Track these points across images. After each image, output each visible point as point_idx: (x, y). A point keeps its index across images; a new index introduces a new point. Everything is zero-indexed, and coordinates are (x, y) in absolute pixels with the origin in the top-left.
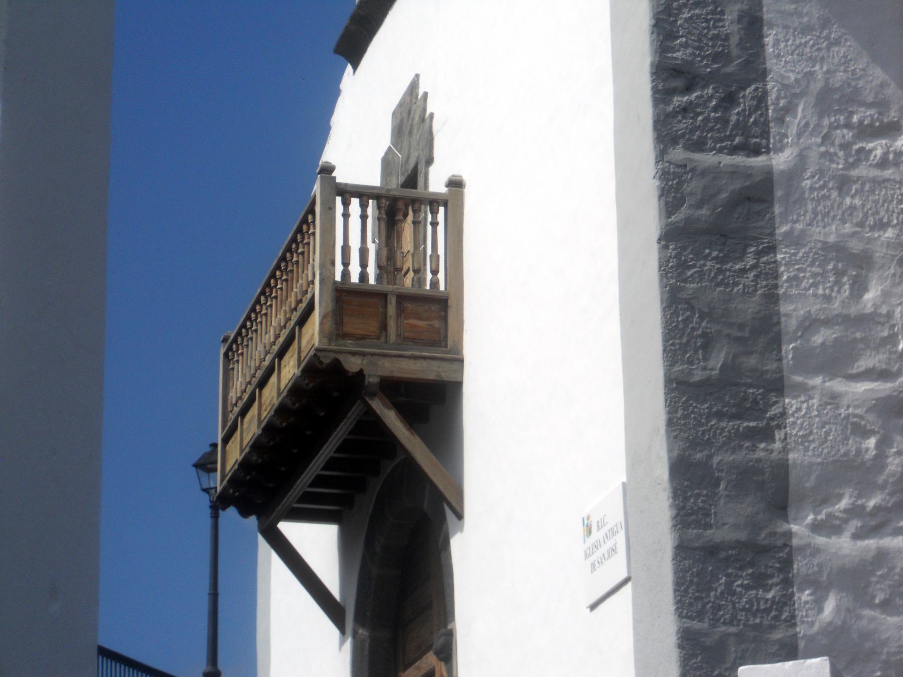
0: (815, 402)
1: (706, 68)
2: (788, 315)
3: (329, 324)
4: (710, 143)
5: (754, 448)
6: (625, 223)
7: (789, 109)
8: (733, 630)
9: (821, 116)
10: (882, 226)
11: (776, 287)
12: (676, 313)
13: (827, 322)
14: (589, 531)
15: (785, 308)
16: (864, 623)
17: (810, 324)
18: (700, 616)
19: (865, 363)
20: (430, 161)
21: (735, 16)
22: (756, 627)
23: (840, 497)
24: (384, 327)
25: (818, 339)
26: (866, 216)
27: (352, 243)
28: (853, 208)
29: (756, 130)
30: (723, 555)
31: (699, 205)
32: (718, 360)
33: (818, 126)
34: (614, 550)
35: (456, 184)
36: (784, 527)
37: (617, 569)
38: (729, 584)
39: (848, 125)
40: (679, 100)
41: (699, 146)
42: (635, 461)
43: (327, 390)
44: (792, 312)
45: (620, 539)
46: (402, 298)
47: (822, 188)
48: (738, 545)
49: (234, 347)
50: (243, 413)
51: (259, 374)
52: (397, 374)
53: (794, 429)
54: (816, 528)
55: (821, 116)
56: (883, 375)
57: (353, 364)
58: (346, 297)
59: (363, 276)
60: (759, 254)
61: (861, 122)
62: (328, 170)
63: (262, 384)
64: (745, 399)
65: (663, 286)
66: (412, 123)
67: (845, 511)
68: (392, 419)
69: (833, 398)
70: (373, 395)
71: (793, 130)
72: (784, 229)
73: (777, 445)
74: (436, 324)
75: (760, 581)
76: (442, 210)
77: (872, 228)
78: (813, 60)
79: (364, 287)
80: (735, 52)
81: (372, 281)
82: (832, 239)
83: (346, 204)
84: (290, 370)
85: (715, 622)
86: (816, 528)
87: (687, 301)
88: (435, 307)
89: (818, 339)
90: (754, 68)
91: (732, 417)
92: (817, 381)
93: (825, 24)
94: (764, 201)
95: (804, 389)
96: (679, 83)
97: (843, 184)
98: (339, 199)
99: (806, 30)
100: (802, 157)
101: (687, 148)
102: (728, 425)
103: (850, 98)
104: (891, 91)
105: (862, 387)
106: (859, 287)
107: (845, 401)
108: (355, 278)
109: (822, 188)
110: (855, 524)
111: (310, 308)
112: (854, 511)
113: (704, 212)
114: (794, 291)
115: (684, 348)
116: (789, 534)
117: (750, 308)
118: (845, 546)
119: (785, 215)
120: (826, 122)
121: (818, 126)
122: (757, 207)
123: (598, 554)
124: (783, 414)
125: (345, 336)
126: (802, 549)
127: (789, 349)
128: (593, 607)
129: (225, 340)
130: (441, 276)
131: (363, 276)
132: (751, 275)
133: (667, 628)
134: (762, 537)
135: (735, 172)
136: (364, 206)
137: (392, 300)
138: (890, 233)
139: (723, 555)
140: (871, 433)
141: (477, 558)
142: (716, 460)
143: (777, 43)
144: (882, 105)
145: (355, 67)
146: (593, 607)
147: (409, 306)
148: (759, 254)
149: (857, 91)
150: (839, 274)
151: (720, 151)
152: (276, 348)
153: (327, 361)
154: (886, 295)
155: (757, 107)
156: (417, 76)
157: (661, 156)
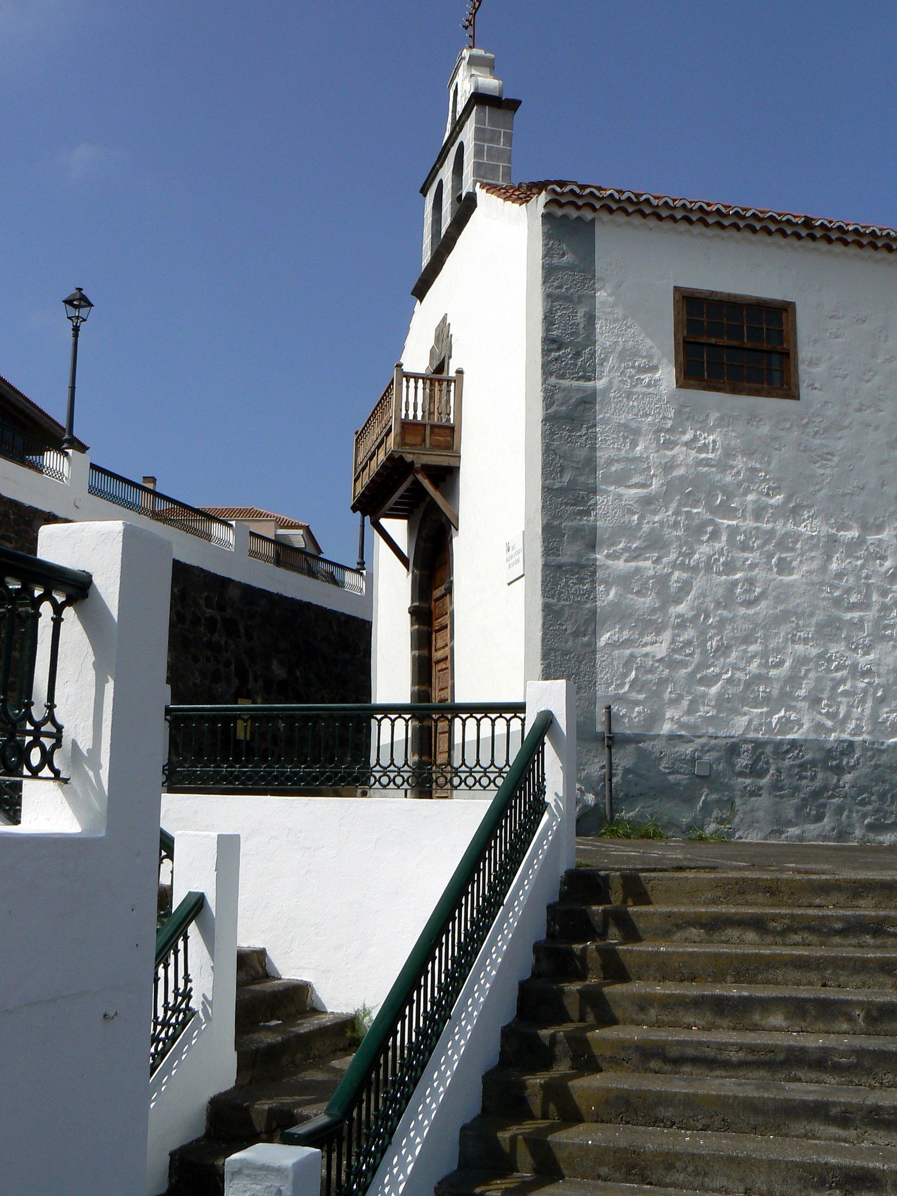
0: (611, 498)
1: (567, 339)
2: (600, 457)
3: (398, 438)
4: (568, 375)
5: (581, 520)
6: (528, 410)
7: (605, 359)
8: (567, 603)
9: (620, 362)
10: (646, 415)
11: (595, 444)
12: (548, 456)
13: (618, 461)
15: (599, 454)
16: (628, 601)
17: (610, 462)
18: (553, 597)
19: (634, 480)
20: (450, 357)
21: (582, 314)
22: (578, 602)
23: (620, 542)
24: (424, 440)
25: (613, 469)
26: (639, 411)
27: (413, 401)
28: (633, 406)
29: (590, 369)
30: (564, 569)
31: (562, 405)
32: (566, 478)
33: (619, 367)
34: (518, 561)
35: (460, 372)
36: (594, 556)
38: (567, 582)
39: (633, 367)
40: (554, 355)
41: (562, 377)
43: (395, 470)
44: (602, 455)
46: (433, 427)
47: (619, 397)
48: (572, 564)
49: (360, 436)
50: (363, 469)
51: (370, 454)
52: (429, 463)
53: (600, 510)
54: (608, 556)
55: (620, 362)
56: (643, 486)
57: (409, 458)
58: (407, 426)
59: (415, 416)
60: (588, 428)
61: (639, 366)
62: (400, 366)
63: (371, 459)
64: (578, 496)
65: (543, 443)
66: (443, 335)
67: (622, 549)
68: (426, 484)
69: (619, 497)
70: (418, 472)
71: (607, 370)
72: (601, 416)
73: (592, 518)
74: (449, 439)
75: (581, 581)
76: (453, 384)
77: (642, 417)
78: (618, 335)
79: (415, 421)
80: (581, 331)
81: (419, 418)
82: (622, 422)
83: (408, 382)
84: (381, 457)
85: (559, 600)
86: (608, 556)
87: (554, 450)
88: (448, 431)
89: (613, 469)
90: (590, 340)
91: (572, 505)
92: (613, 488)
93: (625, 318)
94: (590, 403)
95: (606, 492)
96: (555, 346)
97: (629, 395)
98: (404, 379)
99: (616, 320)
100: (610, 382)
101: (557, 377)
102: (570, 509)
103: (634, 354)
104: (654, 350)
105: (633, 491)
106: (634, 444)
107: (624, 498)
108: (411, 417)
109: (619, 397)
110: (626, 555)
111: (390, 430)
112: (626, 549)
114: (603, 446)
115: (551, 472)
116: (596, 559)
117: (582, 454)
118: (620, 565)
119: (601, 410)
120: (623, 365)
121: (619, 367)
122: (588, 406)
123: (512, 561)
124: (596, 504)
125: (406, 444)
126: (600, 566)
127: (600, 473)
128: (509, 584)
129: (356, 433)
130: (452, 416)
131: (415, 416)
132: (584, 438)
134: (583, 561)
135: (579, 389)
136: (416, 383)
137: (428, 428)
138: (650, 419)
139: (564, 569)
140: (637, 513)
141: (463, 547)
142: (563, 525)
143: (601, 327)
144: (650, 357)
145: (421, 302)
146: (509, 584)
147: (436, 430)
148: (588, 428)
149: (638, 351)
150: (625, 438)
151: (572, 379)
152: (377, 444)
153: (396, 457)
154: (646, 448)
155: (591, 358)
156: (445, 318)
157: (544, 381)
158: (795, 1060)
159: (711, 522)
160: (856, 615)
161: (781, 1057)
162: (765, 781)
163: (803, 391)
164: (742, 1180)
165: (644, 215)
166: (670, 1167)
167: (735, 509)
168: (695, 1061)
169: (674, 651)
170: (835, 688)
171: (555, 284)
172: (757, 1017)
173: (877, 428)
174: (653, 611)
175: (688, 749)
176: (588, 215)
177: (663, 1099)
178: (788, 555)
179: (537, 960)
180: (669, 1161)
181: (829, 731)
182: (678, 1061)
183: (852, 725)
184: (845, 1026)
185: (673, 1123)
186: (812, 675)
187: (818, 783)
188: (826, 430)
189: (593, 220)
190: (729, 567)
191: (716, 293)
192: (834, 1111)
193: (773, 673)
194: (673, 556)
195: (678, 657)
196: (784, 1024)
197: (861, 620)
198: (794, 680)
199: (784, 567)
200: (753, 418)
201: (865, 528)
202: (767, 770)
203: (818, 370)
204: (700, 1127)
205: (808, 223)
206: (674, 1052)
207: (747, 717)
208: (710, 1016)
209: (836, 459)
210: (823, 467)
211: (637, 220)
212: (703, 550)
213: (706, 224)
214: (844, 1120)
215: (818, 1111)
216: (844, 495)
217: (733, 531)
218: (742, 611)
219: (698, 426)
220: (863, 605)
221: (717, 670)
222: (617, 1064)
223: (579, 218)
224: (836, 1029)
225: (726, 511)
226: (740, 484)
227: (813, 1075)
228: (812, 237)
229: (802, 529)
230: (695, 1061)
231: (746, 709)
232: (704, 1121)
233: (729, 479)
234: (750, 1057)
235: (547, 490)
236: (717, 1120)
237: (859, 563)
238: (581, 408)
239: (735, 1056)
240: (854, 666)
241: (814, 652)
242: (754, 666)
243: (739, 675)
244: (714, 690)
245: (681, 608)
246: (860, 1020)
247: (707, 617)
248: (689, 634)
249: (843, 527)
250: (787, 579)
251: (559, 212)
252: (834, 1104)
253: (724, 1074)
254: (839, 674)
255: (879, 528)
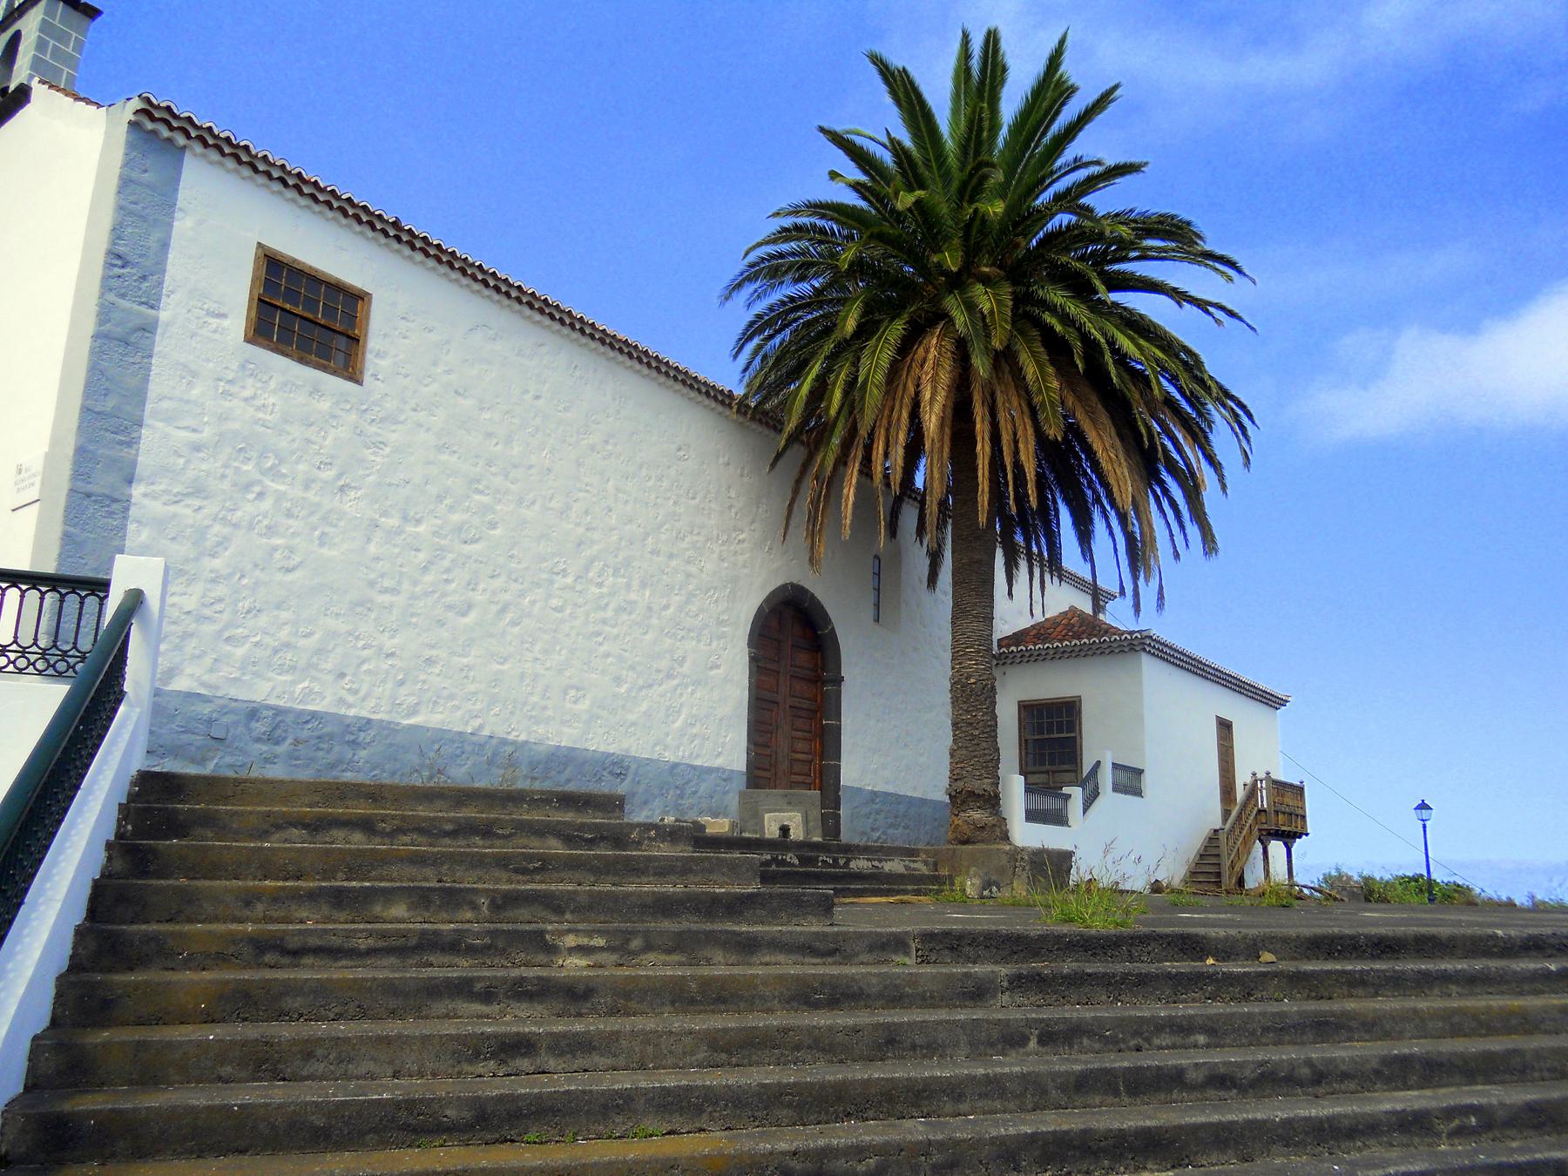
1: (134, 259)
6: (74, 324)
14: (20, 472)
15: (151, 386)
18: (75, 525)
19: (185, 424)
31: (117, 325)
37: (34, 494)
40: (117, 271)
41: (123, 296)
42: (55, 442)
44: (154, 389)
45: (38, 480)
69: (166, 436)
86: (145, 495)
92: (160, 425)
96: (119, 262)
105: (183, 434)
110: (165, 498)
113: (119, 329)
118: (157, 508)
133: (56, 529)
134: (116, 495)
135: (140, 314)
138: (211, 365)
157: (102, 295)
158: (430, 943)
159: (260, 482)
160: (387, 598)
161: (413, 941)
162: (281, 749)
163: (367, 378)
164: (391, 1062)
165: (240, 162)
166: (309, 1056)
167: (285, 476)
168: (317, 951)
169: (204, 605)
170: (359, 666)
171: (132, 198)
172: (377, 909)
173: (428, 430)
174: (187, 560)
175: (206, 710)
176: (181, 140)
177: (289, 988)
178: (328, 529)
179: (109, 859)
180: (308, 1050)
181: (350, 706)
182: (297, 953)
183: (372, 703)
184: (469, 915)
185: (301, 1015)
186: (338, 650)
187: (331, 758)
188: (382, 420)
189: (184, 148)
190: (271, 530)
191: (299, 262)
192: (478, 987)
193: (302, 642)
194: (215, 509)
195: (207, 612)
196: (406, 915)
197: (391, 606)
198: (320, 651)
199: (323, 540)
200: (316, 391)
201: (405, 518)
202: (285, 739)
203: (384, 363)
204: (332, 1016)
205: (396, 224)
206: (294, 943)
207: (271, 684)
208: (326, 910)
209: (388, 450)
210: (374, 453)
211: (231, 164)
212: (247, 509)
213: (301, 193)
214: (487, 996)
215: (462, 989)
216: (390, 485)
217: (280, 496)
218: (279, 576)
219: (259, 385)
220: (394, 591)
221: (246, 632)
222: (224, 960)
223: (169, 140)
224: (460, 918)
225: (274, 473)
226: (293, 453)
227: (446, 959)
228: (398, 239)
229: (346, 507)
230: (317, 951)
231: (271, 675)
232: (336, 1010)
233: (283, 444)
234: (381, 944)
235: (86, 410)
236: (352, 1008)
237: (397, 550)
238: (139, 334)
239: (363, 944)
240: (380, 649)
241: (345, 628)
242: (284, 634)
243: (268, 640)
244: (240, 652)
245: (217, 563)
246: (484, 908)
247: (242, 576)
248: (220, 590)
249: (385, 514)
250: (325, 551)
251: (150, 126)
252: (479, 979)
253: (350, 963)
254: (366, 653)
255: (418, 522)
